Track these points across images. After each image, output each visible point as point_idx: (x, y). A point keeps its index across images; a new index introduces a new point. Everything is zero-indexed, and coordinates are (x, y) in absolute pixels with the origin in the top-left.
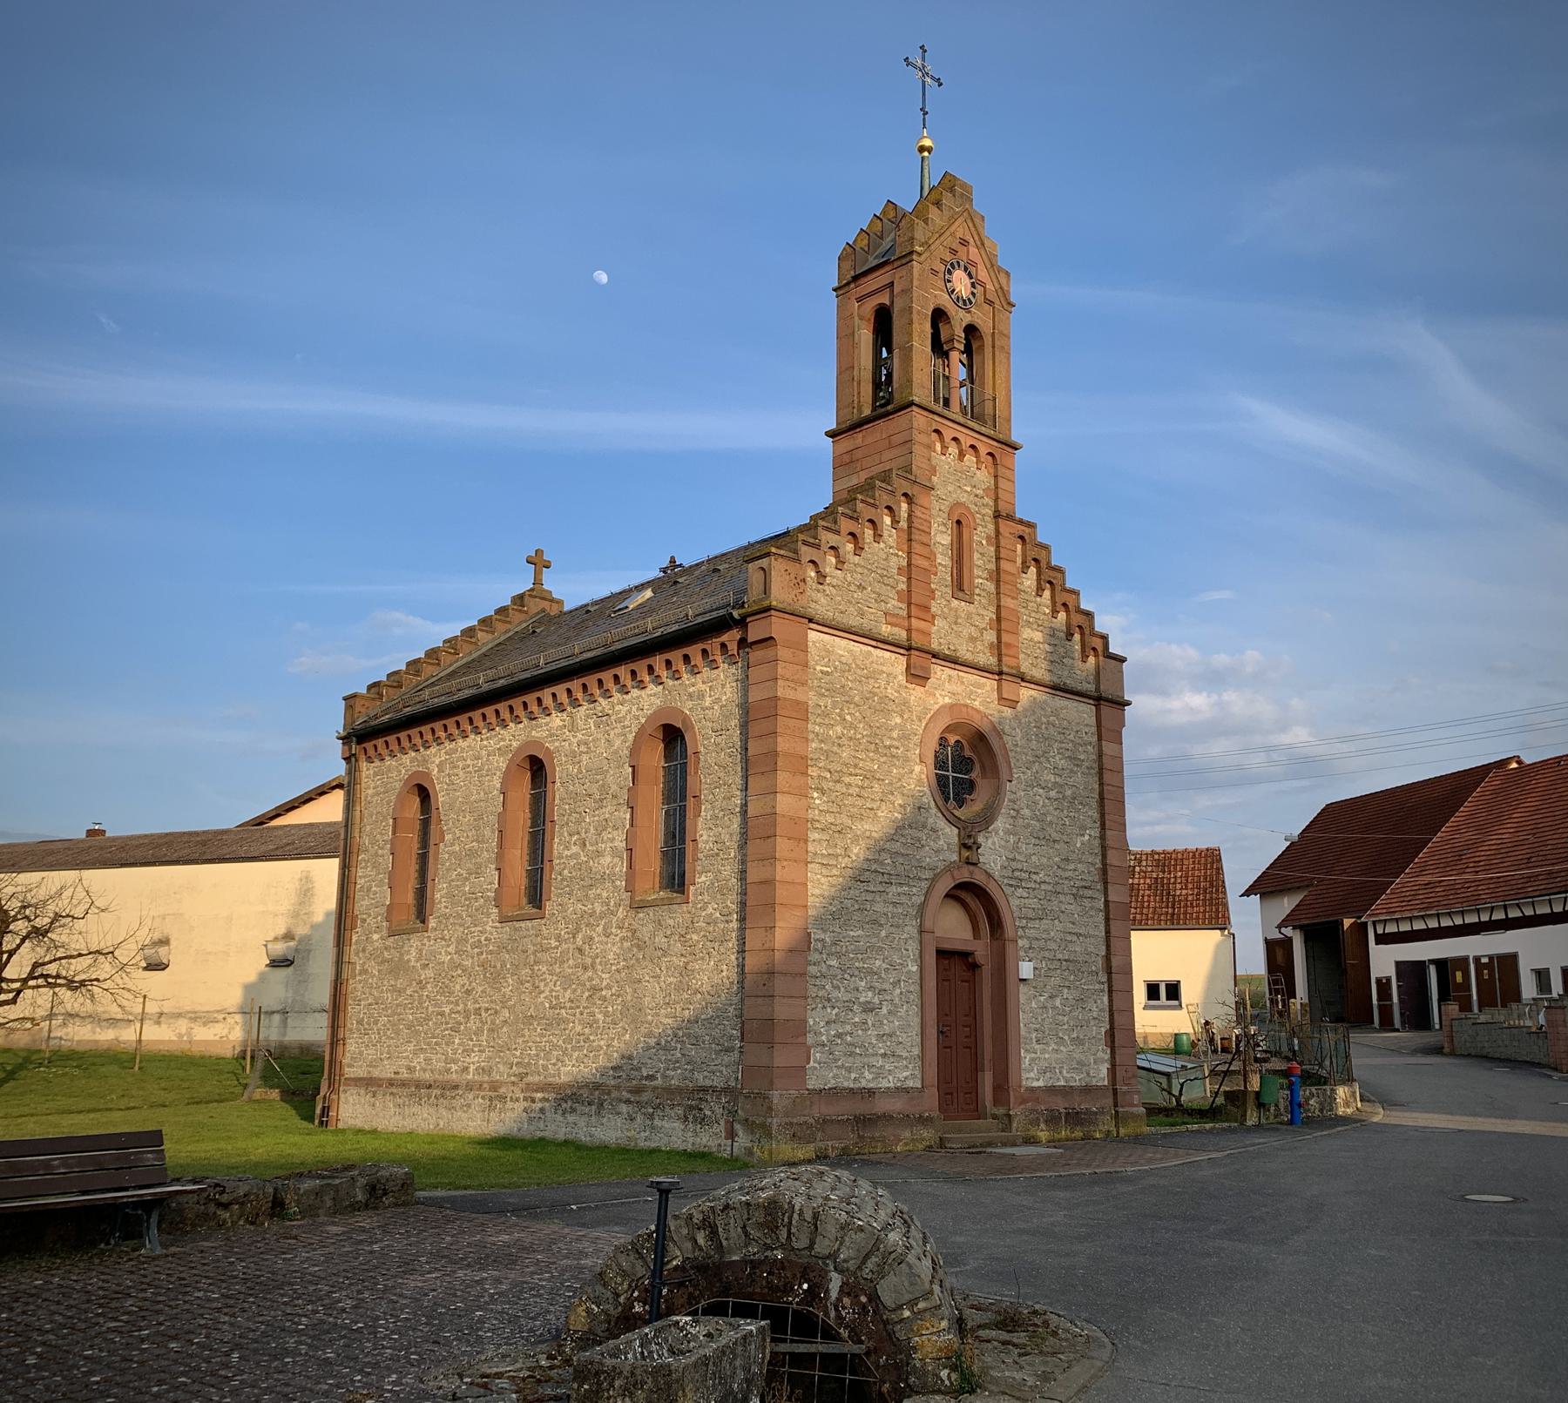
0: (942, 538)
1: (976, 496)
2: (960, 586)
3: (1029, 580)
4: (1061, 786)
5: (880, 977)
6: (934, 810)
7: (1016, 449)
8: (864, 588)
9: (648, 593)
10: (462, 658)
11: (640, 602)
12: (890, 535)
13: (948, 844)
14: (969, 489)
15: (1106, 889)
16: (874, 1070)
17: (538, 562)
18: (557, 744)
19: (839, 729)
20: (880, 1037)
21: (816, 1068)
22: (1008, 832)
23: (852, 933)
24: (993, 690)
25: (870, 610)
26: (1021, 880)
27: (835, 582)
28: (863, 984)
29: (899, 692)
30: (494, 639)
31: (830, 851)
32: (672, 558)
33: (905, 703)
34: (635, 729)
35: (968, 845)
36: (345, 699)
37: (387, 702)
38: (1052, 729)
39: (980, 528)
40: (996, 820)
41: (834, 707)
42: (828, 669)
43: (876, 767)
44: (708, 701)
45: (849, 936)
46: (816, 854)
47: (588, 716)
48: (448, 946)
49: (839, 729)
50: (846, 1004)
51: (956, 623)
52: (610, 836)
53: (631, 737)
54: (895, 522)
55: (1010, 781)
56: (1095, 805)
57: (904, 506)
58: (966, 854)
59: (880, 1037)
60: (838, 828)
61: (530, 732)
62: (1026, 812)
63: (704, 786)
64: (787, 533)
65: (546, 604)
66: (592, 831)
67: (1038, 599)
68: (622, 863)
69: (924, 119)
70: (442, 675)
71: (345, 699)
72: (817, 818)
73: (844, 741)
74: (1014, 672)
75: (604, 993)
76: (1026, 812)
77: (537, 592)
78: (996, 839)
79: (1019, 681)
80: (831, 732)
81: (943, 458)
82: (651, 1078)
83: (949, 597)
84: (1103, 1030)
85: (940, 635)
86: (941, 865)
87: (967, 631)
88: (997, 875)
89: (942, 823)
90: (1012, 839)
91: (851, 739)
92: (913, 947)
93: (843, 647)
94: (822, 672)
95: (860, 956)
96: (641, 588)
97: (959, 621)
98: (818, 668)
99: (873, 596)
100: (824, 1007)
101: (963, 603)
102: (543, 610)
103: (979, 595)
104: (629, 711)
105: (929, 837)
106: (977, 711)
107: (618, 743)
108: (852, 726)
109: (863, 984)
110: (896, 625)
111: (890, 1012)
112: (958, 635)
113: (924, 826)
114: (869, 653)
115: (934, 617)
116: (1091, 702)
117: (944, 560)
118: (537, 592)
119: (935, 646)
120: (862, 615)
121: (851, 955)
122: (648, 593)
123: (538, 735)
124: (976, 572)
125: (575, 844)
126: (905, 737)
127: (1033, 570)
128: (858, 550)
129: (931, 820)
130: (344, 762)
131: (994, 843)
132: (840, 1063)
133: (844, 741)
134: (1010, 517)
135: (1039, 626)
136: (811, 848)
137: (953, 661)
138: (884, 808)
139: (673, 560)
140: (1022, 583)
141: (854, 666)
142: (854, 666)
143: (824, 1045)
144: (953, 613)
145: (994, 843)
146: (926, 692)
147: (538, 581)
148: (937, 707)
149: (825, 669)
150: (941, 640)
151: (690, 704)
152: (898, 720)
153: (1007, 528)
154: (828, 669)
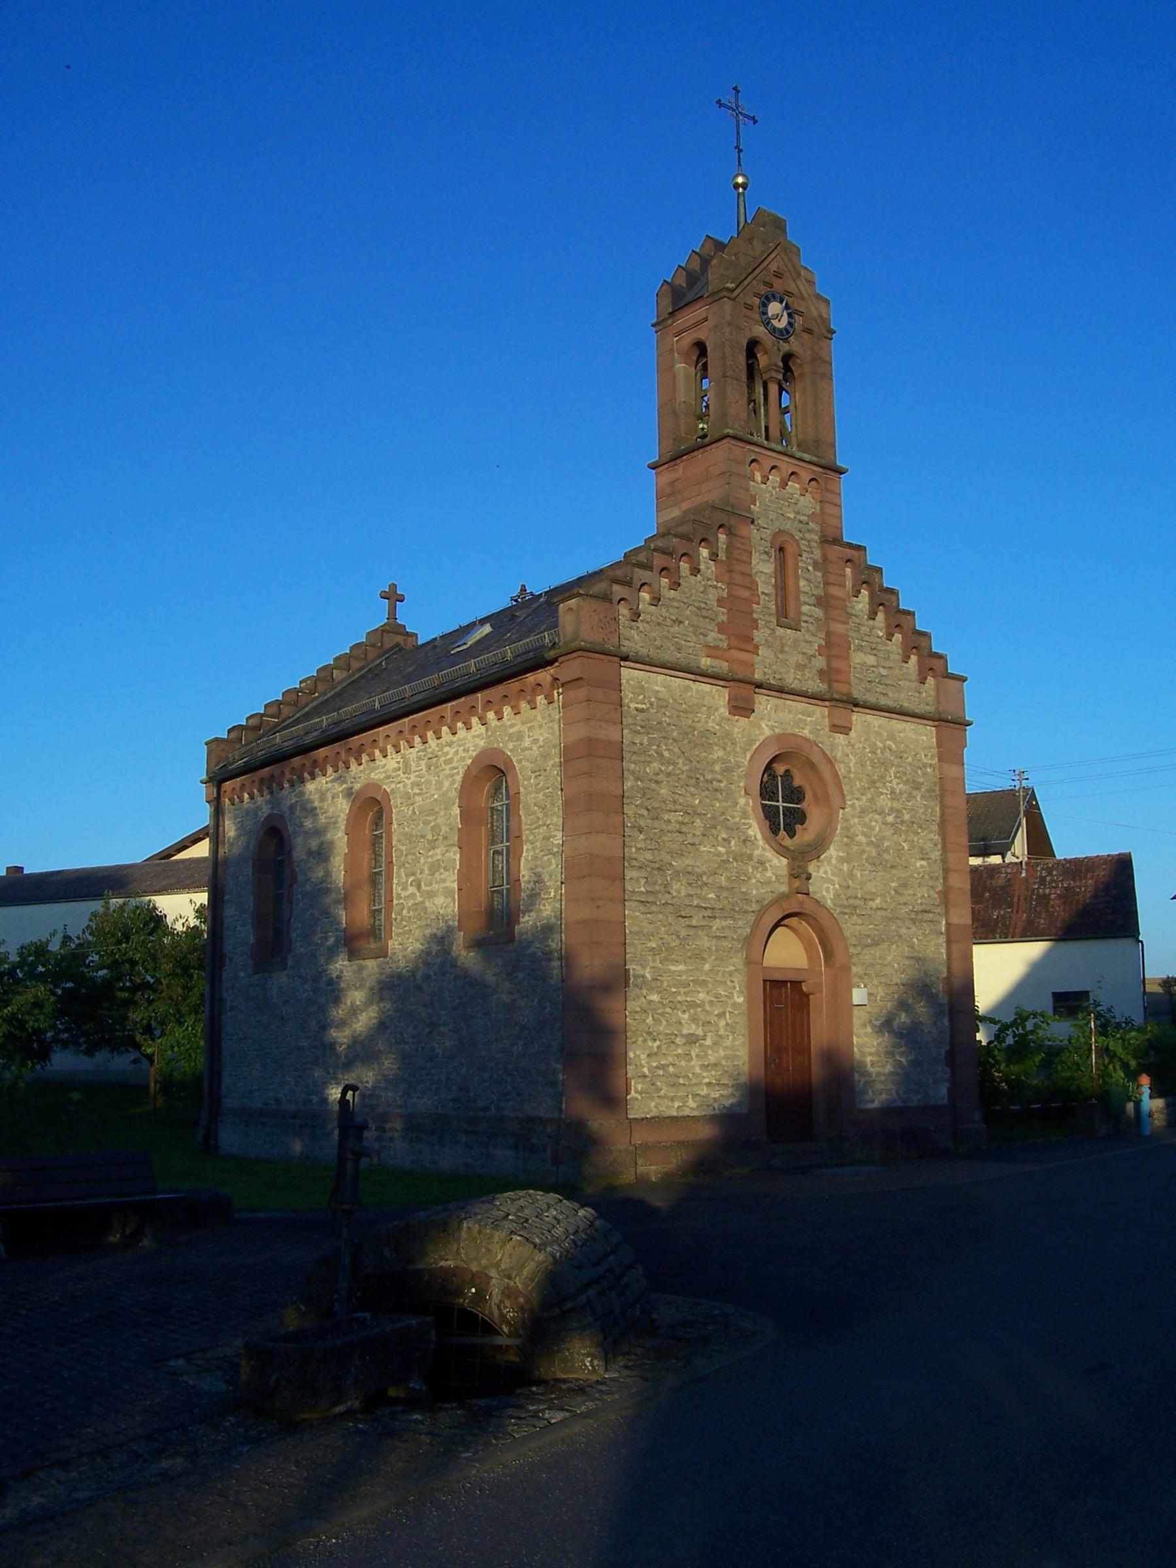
0: (763, 568)
1: (801, 522)
2: (785, 616)
3: (862, 602)
4: (898, 811)
5: (704, 1010)
6: (761, 842)
7: (842, 473)
8: (681, 622)
9: (487, 629)
10: (318, 697)
11: (478, 638)
12: (708, 567)
13: (776, 876)
14: (792, 516)
15: (947, 912)
16: (698, 1098)
17: (393, 597)
18: (393, 786)
19: (656, 765)
20: (705, 1067)
21: (637, 1099)
22: (840, 859)
23: (673, 968)
24: (823, 717)
25: (688, 644)
26: (855, 907)
27: (648, 618)
28: (686, 1016)
29: (720, 725)
30: (350, 676)
31: (649, 889)
32: (523, 586)
33: (728, 735)
34: (462, 771)
35: (799, 875)
36: (207, 744)
37: (246, 745)
38: (887, 754)
39: (805, 555)
40: (828, 848)
41: (650, 744)
42: (644, 706)
43: (697, 801)
44: (527, 742)
45: (670, 971)
46: (633, 892)
47: (419, 758)
48: (305, 983)
49: (656, 765)
50: (669, 1037)
51: (782, 652)
52: (443, 877)
53: (459, 778)
54: (714, 556)
55: (843, 808)
56: (935, 828)
57: (722, 537)
58: (797, 883)
59: (705, 1067)
60: (657, 865)
61: (369, 774)
62: (861, 838)
63: (524, 827)
64: (601, 571)
65: (399, 639)
66: (427, 872)
67: (871, 622)
68: (454, 904)
69: (738, 139)
70: (298, 715)
71: (207, 744)
72: (635, 856)
73: (661, 777)
74: (845, 698)
75: (442, 1029)
76: (861, 838)
77: (393, 628)
78: (828, 869)
79: (851, 706)
80: (648, 770)
81: (763, 486)
82: (486, 1109)
83: (773, 625)
84: (943, 1052)
85: (764, 665)
86: (769, 897)
87: (795, 657)
88: (829, 903)
89: (770, 854)
90: (845, 867)
91: (669, 775)
92: (738, 980)
93: (659, 682)
94: (637, 709)
95: (682, 990)
96: (483, 621)
97: (786, 649)
98: (633, 705)
99: (691, 629)
100: (645, 1041)
101: (789, 631)
102: (397, 645)
103: (806, 622)
104: (457, 753)
105: (755, 868)
106: (806, 740)
107: (447, 784)
108: (669, 762)
109: (686, 1016)
110: (716, 657)
111: (715, 1043)
112: (784, 662)
113: (750, 857)
114: (688, 688)
115: (757, 647)
116: (931, 723)
117: (765, 586)
118: (393, 628)
119: (758, 676)
120: (679, 649)
121: (674, 990)
122: (487, 629)
123: (376, 777)
124: (803, 598)
125: (411, 885)
126: (728, 770)
127: (865, 593)
128: (675, 585)
129: (757, 853)
130: (207, 804)
131: (826, 872)
132: (662, 1093)
133: (661, 777)
134: (837, 541)
135: (872, 649)
136: (629, 887)
137: (781, 690)
138: (706, 842)
139: (523, 589)
140: (853, 607)
141: (671, 701)
142: (671, 701)
143: (645, 1076)
144: (778, 642)
145: (826, 872)
146: (751, 723)
147: (392, 614)
148: (762, 738)
149: (640, 706)
150: (766, 670)
151: (511, 745)
152: (721, 753)
153: (835, 552)
154: (644, 706)
